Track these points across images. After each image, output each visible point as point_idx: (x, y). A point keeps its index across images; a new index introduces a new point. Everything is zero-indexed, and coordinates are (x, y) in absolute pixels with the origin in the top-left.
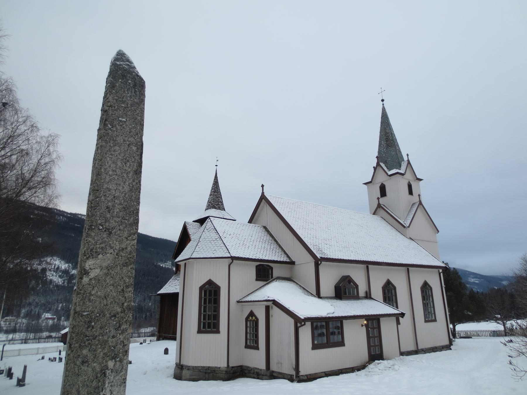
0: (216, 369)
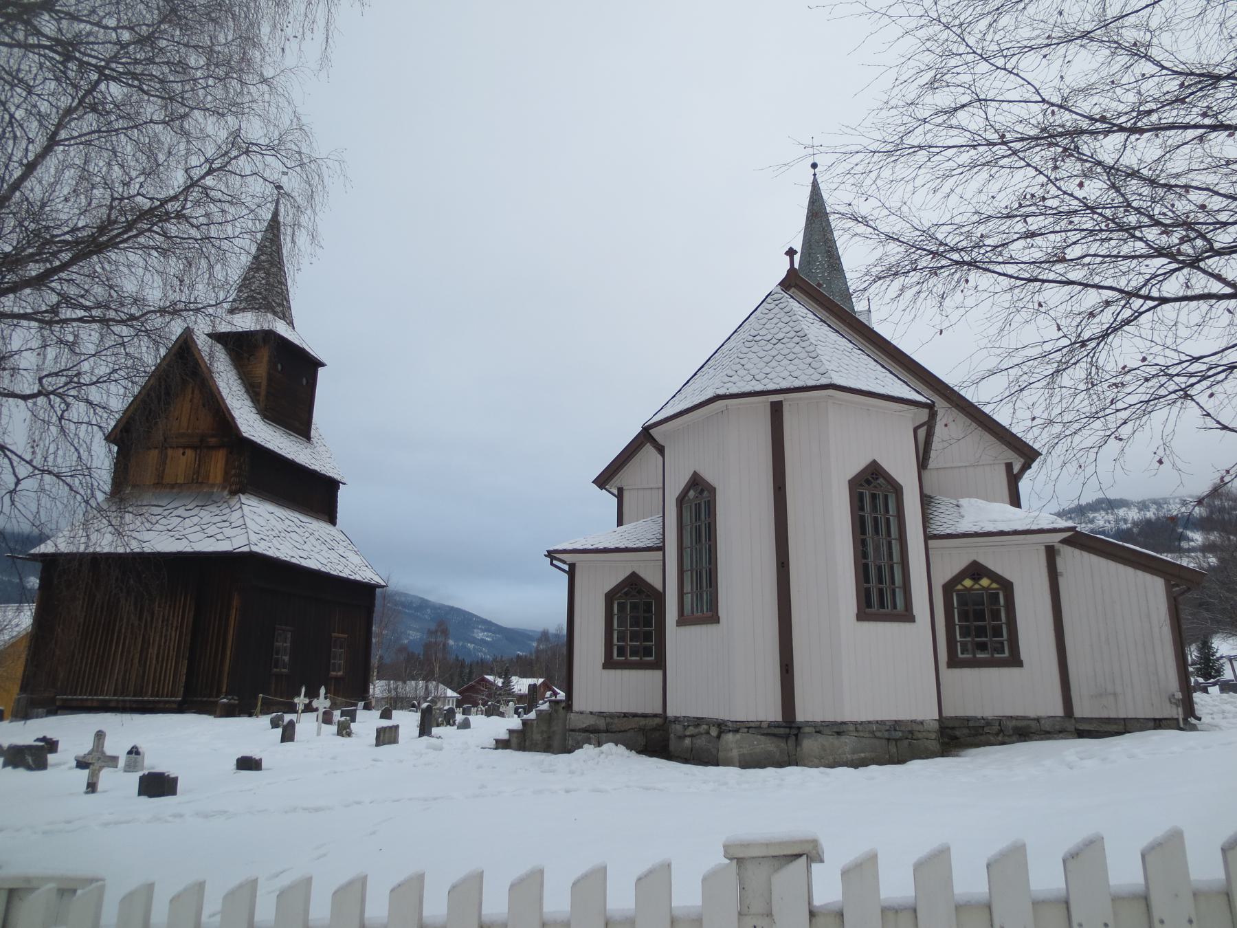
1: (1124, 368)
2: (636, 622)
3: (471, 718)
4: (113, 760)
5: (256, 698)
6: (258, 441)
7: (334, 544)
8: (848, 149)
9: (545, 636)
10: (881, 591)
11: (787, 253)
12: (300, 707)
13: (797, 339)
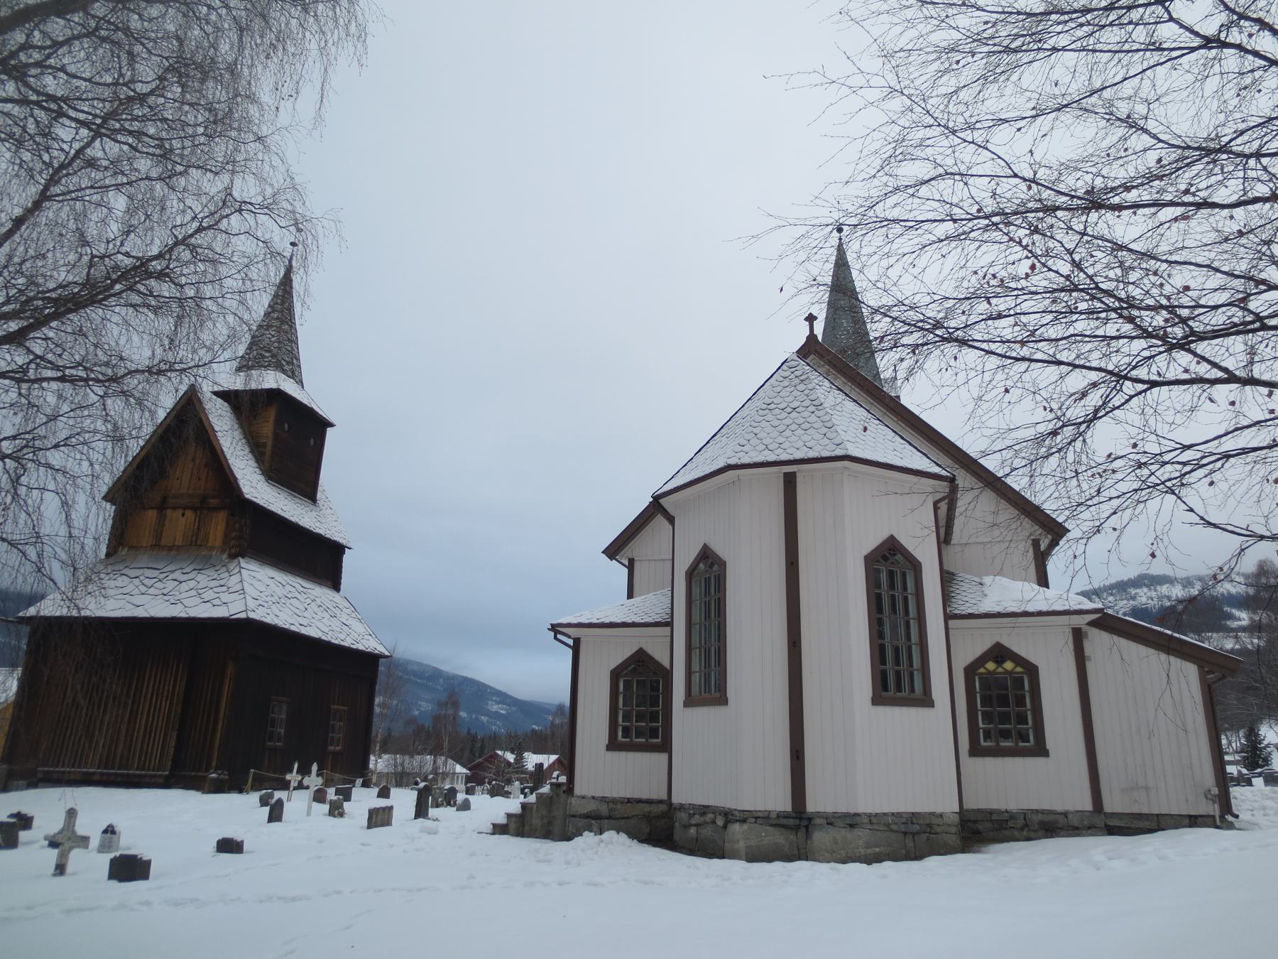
0: (935, 821)
1: (1109, 456)
2: (641, 704)
4: (84, 841)
5: (248, 773)
6: (261, 502)
7: (337, 611)
8: (818, 222)
10: (898, 674)
11: (806, 319)
12: (294, 784)
13: (812, 408)
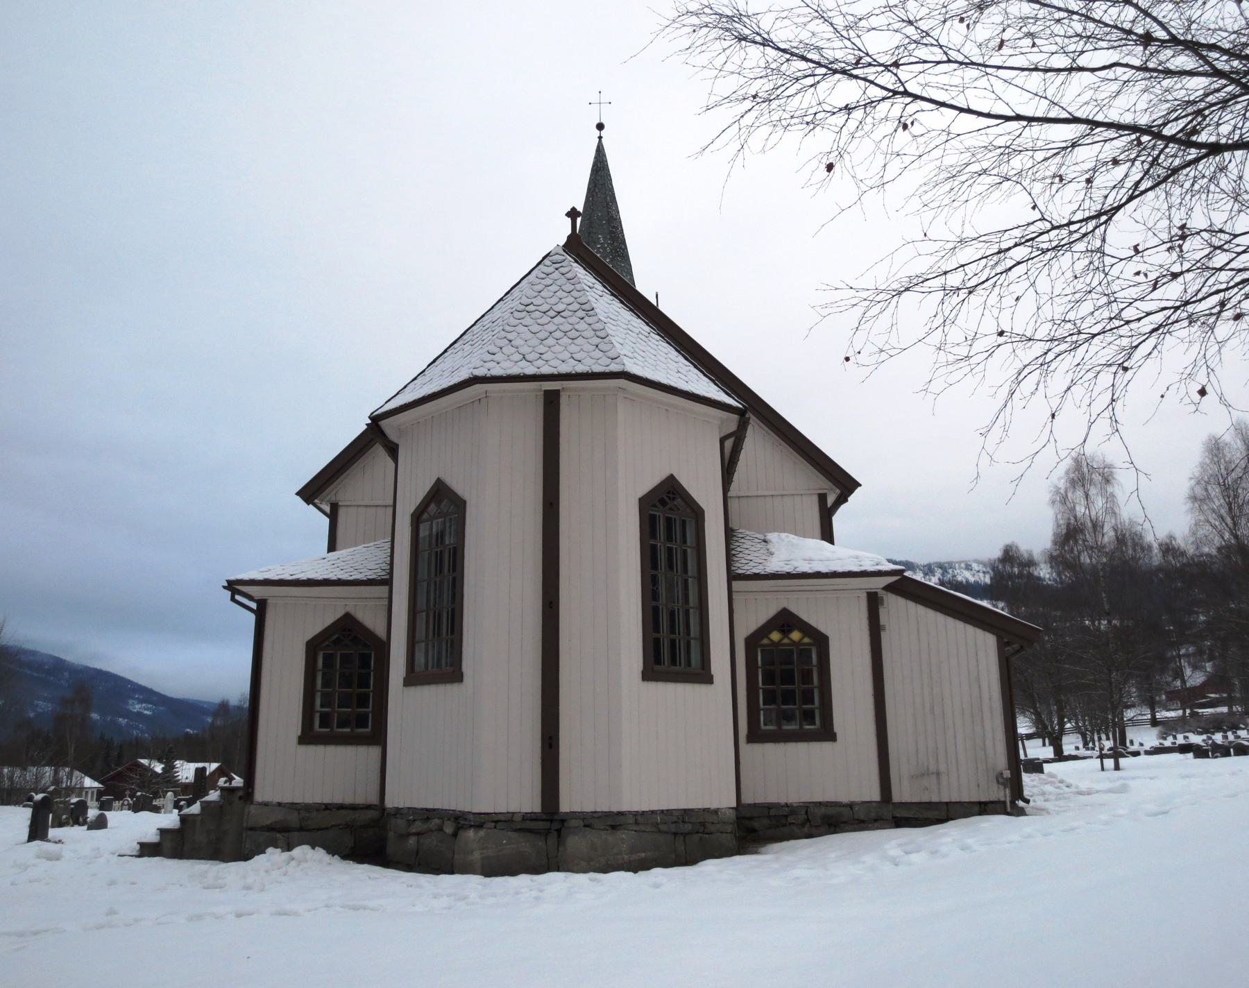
2: (347, 681)
3: (109, 815)
9: (223, 707)
11: (568, 215)
